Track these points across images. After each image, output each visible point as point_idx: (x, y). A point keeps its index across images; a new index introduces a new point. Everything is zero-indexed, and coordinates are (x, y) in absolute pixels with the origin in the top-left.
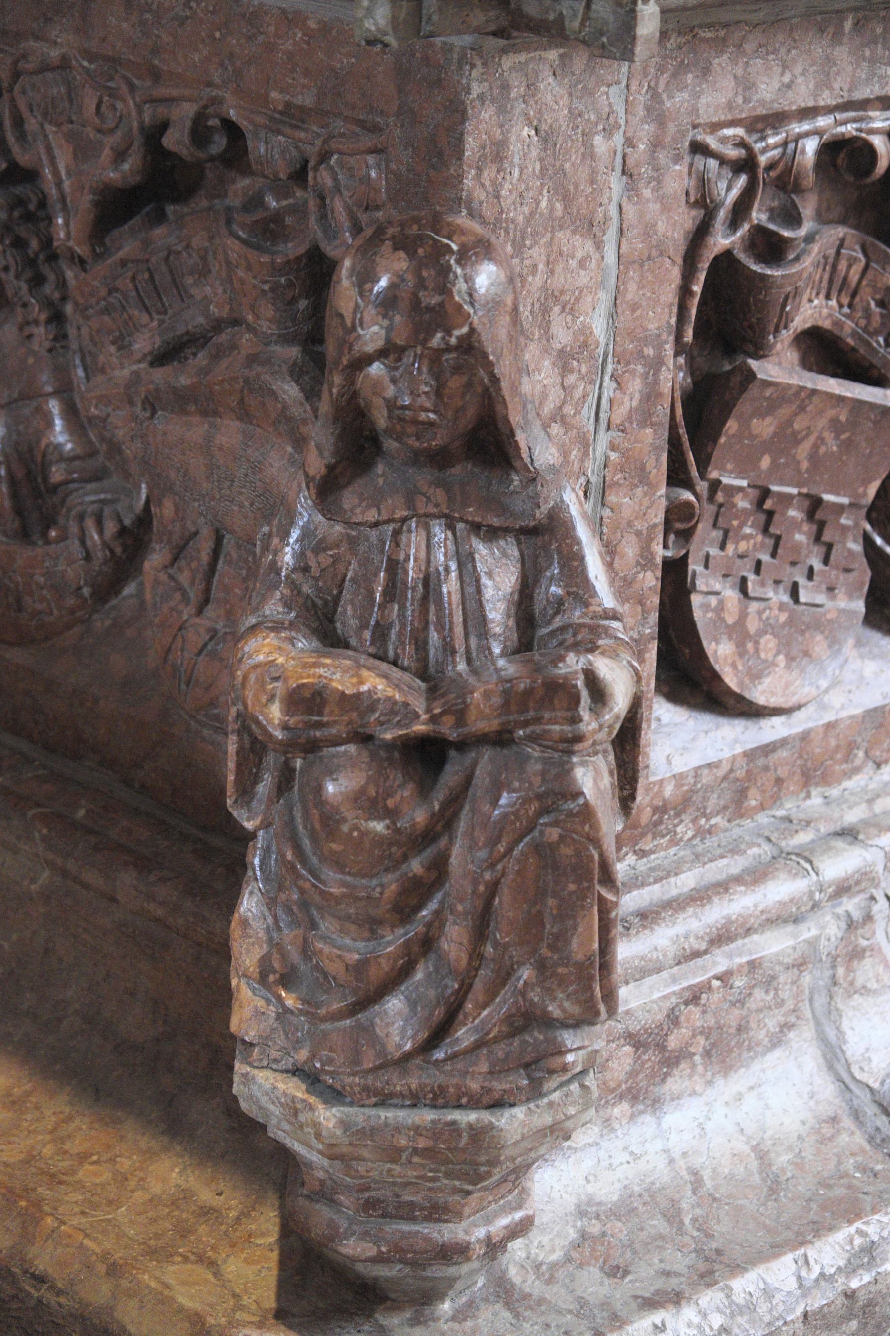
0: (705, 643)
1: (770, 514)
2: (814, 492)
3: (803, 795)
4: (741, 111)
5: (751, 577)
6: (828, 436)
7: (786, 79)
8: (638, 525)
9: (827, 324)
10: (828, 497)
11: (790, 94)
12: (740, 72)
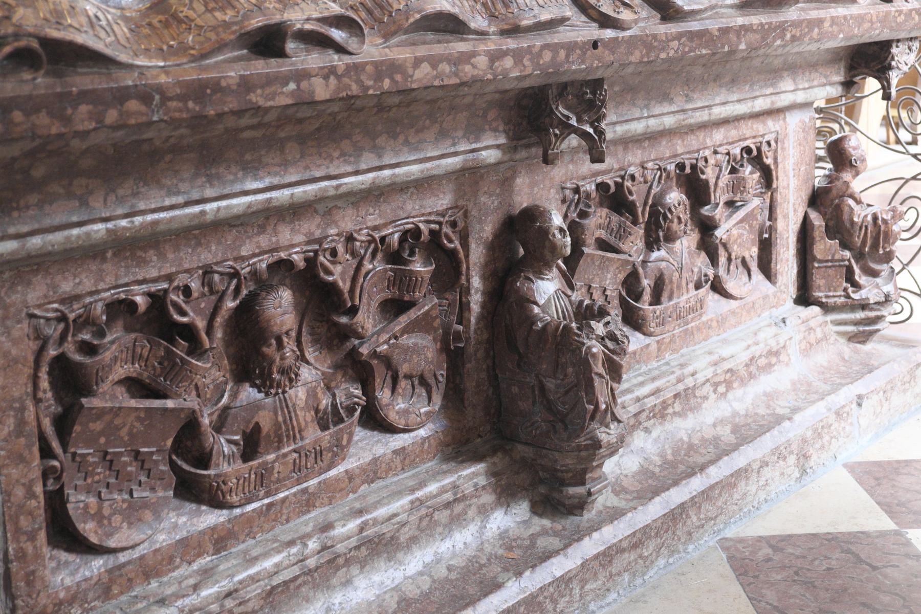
0: (77, 525)
1: (111, 461)
2: (134, 448)
5: (104, 490)
6: (137, 424)
7: (77, 280)
8: (23, 481)
9: (134, 375)
10: (142, 450)
11: (80, 287)
12: (49, 282)
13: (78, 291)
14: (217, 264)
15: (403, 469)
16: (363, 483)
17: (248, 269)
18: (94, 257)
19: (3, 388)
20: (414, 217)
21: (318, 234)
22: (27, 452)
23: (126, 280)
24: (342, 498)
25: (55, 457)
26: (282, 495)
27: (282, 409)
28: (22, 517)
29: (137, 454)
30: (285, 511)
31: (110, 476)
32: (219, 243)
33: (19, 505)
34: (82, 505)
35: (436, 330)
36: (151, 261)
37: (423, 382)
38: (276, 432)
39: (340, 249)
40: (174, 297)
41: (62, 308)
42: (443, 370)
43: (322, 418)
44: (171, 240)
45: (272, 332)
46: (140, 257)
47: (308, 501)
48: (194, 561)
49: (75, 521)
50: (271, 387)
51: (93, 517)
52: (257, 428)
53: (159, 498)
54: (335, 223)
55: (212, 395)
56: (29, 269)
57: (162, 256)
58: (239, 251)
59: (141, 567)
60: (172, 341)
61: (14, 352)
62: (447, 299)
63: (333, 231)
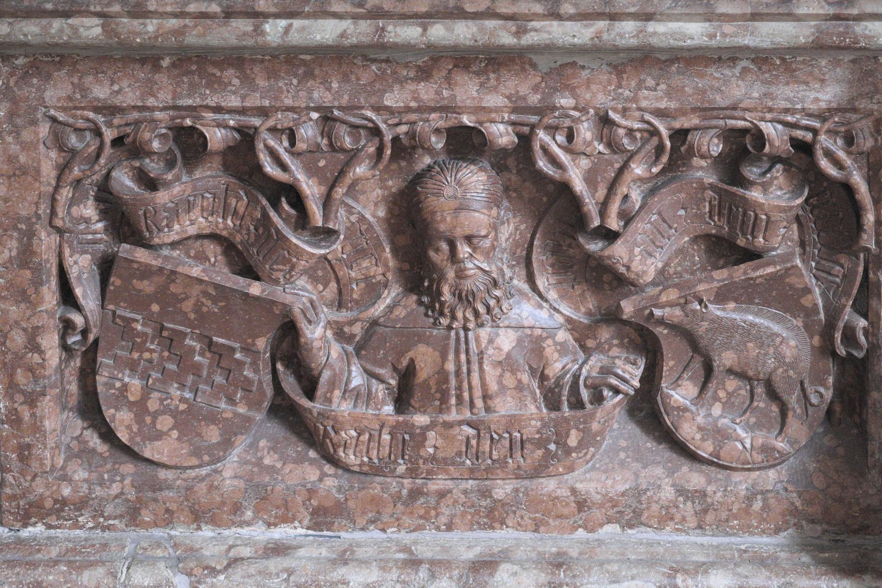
3: (195, 526)
4: (81, 102)
7: (116, 87)
9: (225, 233)
11: (120, 97)
12: (76, 81)
13: (118, 101)
16: (609, 521)
17: (403, 129)
18: (143, 61)
19: (6, 200)
21: (534, 99)
22: (33, 290)
23: (189, 102)
24: (561, 530)
25: (78, 308)
27: (457, 352)
28: (19, 371)
29: (210, 344)
30: (443, 509)
31: (169, 359)
32: (345, 78)
33: (16, 354)
34: (118, 384)
37: (773, 394)
38: (438, 383)
39: (586, 131)
40: (272, 143)
43: (551, 390)
44: (262, 61)
45: (437, 230)
47: (491, 511)
48: (275, 525)
50: (442, 314)
51: (131, 405)
53: (236, 414)
55: (361, 295)
56: (50, 59)
58: (382, 97)
59: (187, 500)
61: (23, 159)
62: (842, 266)
63: (565, 101)
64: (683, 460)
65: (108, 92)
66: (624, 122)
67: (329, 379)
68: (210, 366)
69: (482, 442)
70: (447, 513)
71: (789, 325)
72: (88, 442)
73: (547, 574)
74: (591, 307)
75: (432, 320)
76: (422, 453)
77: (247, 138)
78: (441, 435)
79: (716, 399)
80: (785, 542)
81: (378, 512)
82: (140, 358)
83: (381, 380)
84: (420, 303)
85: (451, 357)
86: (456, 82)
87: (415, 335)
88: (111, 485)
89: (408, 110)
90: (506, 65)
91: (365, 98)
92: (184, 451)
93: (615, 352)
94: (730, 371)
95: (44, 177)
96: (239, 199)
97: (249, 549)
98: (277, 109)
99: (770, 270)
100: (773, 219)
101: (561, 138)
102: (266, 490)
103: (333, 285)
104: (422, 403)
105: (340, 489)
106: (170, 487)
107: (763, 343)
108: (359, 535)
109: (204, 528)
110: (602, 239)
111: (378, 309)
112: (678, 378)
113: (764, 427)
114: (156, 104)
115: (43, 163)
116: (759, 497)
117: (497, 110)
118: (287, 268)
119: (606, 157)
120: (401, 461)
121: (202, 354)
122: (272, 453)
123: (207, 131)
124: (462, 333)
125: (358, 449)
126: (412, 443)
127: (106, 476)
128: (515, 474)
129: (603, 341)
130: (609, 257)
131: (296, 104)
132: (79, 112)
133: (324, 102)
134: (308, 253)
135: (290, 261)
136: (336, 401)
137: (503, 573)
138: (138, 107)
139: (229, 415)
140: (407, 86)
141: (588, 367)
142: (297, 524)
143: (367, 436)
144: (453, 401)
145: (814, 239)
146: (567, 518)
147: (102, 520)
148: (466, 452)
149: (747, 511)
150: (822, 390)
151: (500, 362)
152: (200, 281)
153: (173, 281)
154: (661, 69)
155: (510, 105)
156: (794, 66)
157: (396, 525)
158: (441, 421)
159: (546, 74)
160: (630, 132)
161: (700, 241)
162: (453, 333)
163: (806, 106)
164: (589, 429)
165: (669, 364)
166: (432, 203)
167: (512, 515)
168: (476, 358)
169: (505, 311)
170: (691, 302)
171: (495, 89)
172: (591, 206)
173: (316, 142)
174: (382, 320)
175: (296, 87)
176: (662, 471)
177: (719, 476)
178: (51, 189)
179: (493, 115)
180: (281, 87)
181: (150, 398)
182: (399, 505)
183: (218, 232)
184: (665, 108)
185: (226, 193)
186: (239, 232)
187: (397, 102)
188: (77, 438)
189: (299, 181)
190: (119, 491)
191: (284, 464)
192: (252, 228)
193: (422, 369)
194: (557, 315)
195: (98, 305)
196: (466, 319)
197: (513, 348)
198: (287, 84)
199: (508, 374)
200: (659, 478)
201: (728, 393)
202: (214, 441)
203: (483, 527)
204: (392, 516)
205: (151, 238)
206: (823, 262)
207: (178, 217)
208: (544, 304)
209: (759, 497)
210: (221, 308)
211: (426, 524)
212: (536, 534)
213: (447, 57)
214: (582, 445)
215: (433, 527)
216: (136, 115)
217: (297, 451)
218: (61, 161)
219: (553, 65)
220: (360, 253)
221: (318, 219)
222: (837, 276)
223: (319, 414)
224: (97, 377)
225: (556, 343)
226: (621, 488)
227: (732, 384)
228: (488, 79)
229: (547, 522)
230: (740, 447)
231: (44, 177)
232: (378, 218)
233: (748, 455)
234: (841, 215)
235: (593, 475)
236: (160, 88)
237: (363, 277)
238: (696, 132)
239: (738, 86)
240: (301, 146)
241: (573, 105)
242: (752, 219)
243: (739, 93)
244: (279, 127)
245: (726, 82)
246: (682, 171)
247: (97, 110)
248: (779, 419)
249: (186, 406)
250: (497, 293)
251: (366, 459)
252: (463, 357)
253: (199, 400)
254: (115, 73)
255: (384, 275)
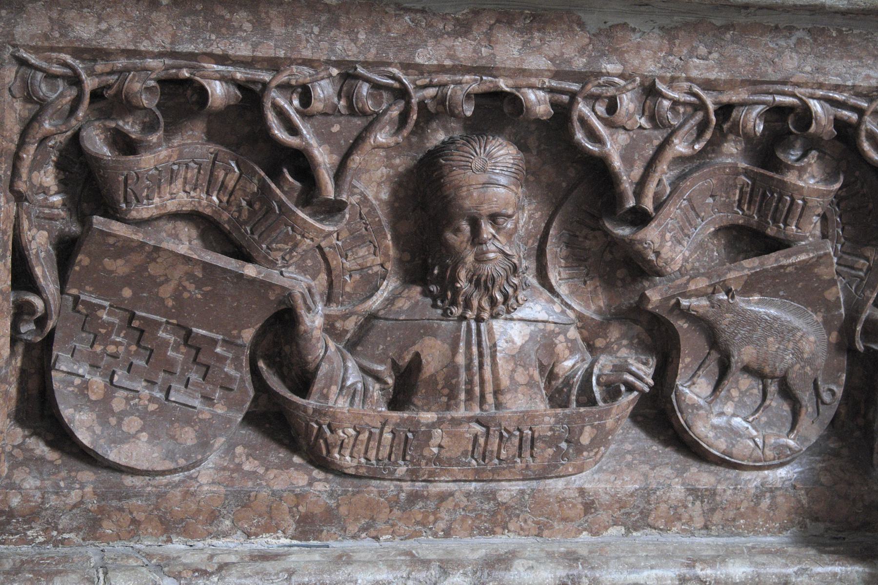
4: (58, 42)
7: (104, 26)
9: (208, 211)
12: (55, 15)
13: (104, 43)
14: (366, 64)
15: (706, 527)
16: (615, 524)
17: (431, 92)
20: (798, 85)
21: (579, 63)
23: (191, 48)
25: (37, 290)
26: (443, 487)
29: (188, 334)
30: (444, 515)
31: (137, 354)
32: (373, 30)
34: (77, 381)
35: (830, 307)
36: (241, 28)
37: (787, 392)
39: (628, 103)
40: (282, 102)
41: (79, 65)
42: (837, 384)
43: (559, 391)
45: (461, 208)
46: (222, 17)
49: (59, 399)
50: (454, 303)
52: (417, 362)
53: (215, 415)
54: (620, 55)
55: (355, 288)
57: (262, 27)
58: (413, 54)
60: (275, 175)
63: (611, 67)
64: (690, 461)
65: (94, 31)
66: (671, 94)
67: (327, 373)
68: (185, 362)
69: (491, 439)
70: (447, 518)
71: (809, 321)
72: (32, 450)
73: (565, 567)
74: (602, 305)
75: (439, 311)
76: (426, 453)
77: (251, 97)
78: (448, 433)
79: (729, 398)
80: (786, 540)
81: (372, 518)
82: (104, 351)
83: (378, 378)
84: (426, 293)
85: (462, 349)
86: (497, 40)
87: (424, 327)
88: (69, 493)
89: (441, 69)
90: (554, 23)
91: (395, 54)
92: (156, 455)
93: (624, 352)
94: (747, 369)
95: (7, 131)
96: (228, 171)
97: (508, 382)
98: (291, 61)
99: (803, 257)
100: (809, 204)
101: (601, 109)
102: (249, 496)
103: (323, 277)
104: (425, 401)
105: (331, 495)
106: (137, 495)
107: (783, 339)
108: (349, 544)
109: (174, 540)
110: (628, 226)
111: (376, 302)
112: (693, 376)
113: (776, 426)
114: (150, 49)
115: (7, 114)
116: (768, 495)
117: (538, 73)
118: (287, 247)
119: (646, 132)
120: (401, 462)
121: (176, 349)
122: (251, 459)
123: (208, 84)
124: (473, 325)
125: (356, 449)
126: (415, 442)
127: (62, 484)
128: (522, 474)
129: (613, 340)
130: (641, 242)
131: (316, 57)
132: (54, 55)
133: (348, 56)
134: (316, 228)
135: (293, 238)
136: (332, 397)
137: (518, 571)
138: (129, 51)
139: (206, 416)
140: (443, 42)
141: (599, 366)
142: (280, 534)
143: (367, 434)
144: (463, 396)
145: (838, 232)
146: (572, 521)
147: (55, 533)
148: (473, 452)
149: (754, 510)
150: (834, 388)
151: (513, 356)
152: (187, 259)
153: (154, 260)
154: (714, 35)
155: (553, 68)
156: (849, 39)
157: (390, 531)
158: (449, 417)
159: (594, 35)
160: (675, 103)
161: (720, 234)
162: (464, 324)
163: (857, 83)
164: (603, 426)
165: (686, 361)
166: (458, 177)
167: (515, 519)
168: (489, 351)
169: (521, 302)
170: (720, 292)
171: (539, 48)
172: (627, 185)
173: (333, 103)
174: (381, 313)
175: (317, 36)
176: (671, 471)
177: (728, 475)
178: (13, 147)
179: (533, 80)
180: (299, 36)
181: (115, 397)
182: (395, 510)
183: (200, 209)
184: (715, 80)
185: (214, 164)
186: (225, 209)
187: (429, 59)
188: (18, 446)
189: (311, 145)
190: (79, 499)
191: (267, 470)
192: (244, 203)
193: (428, 363)
194: (568, 311)
195: (57, 289)
196: (481, 308)
197: (526, 342)
198: (307, 32)
199: (520, 370)
200: (669, 478)
201: (741, 392)
202: (189, 443)
203: (484, 532)
204: (386, 522)
205: (128, 211)
206: (846, 257)
207: (159, 188)
208: (556, 299)
209: (768, 495)
210: (205, 295)
211: (423, 530)
212: (538, 539)
213: (490, 10)
214: (596, 442)
215: (429, 533)
216: (121, 63)
217: (279, 457)
218: (26, 114)
219: (603, 27)
220: (357, 240)
221: (329, 191)
222: (861, 270)
223: (315, 410)
224: (53, 373)
225: (567, 340)
226: (631, 487)
227: (746, 382)
228: (532, 38)
229: (552, 525)
230: (751, 444)
231: (7, 131)
232: (380, 200)
233: (760, 453)
234: (871, 206)
235: (603, 476)
236: (158, 30)
237: (358, 267)
238: (742, 109)
239: (791, 58)
240: (317, 105)
241: (620, 72)
242: (788, 205)
243: (791, 66)
244: (293, 82)
245: (780, 54)
246: (711, 159)
247: (77, 53)
248: (790, 418)
249: (156, 406)
250: (515, 281)
251: (363, 460)
252: (475, 349)
253: (173, 399)
254: (104, 8)
255: (382, 265)
